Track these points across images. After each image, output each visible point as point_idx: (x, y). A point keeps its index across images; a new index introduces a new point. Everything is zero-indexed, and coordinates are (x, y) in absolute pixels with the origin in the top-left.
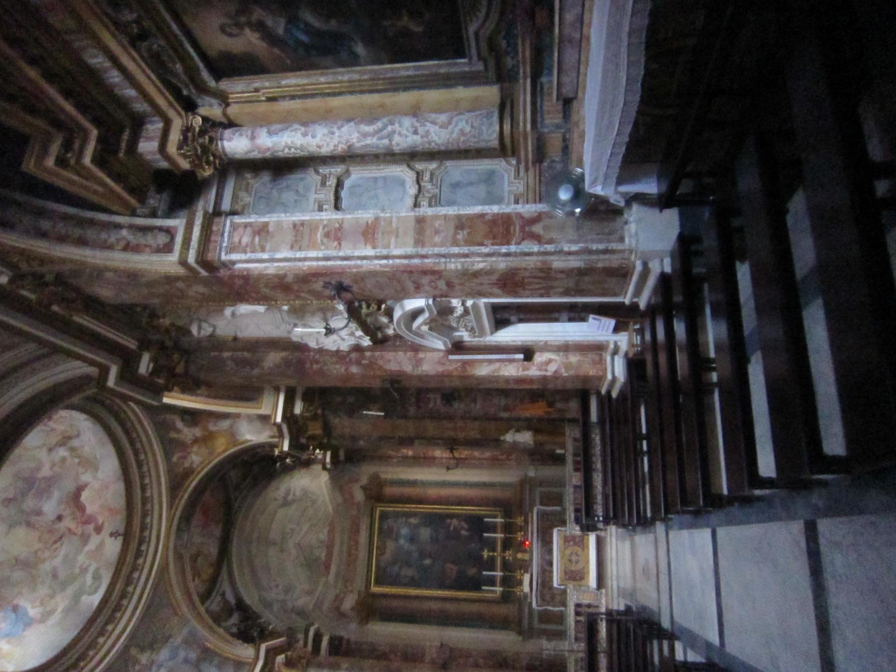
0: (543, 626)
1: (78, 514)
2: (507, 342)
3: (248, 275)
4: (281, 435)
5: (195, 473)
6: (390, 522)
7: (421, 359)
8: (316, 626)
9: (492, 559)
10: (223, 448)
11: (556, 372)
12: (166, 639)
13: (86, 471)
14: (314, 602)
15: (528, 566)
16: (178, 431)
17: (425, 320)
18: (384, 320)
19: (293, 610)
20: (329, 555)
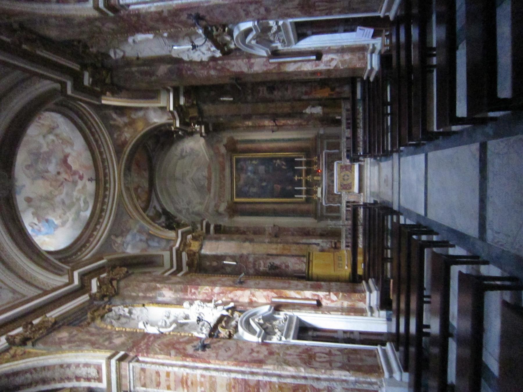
1: (68, 171)
4: (174, 118)
6: (242, 163)
8: (207, 220)
11: (336, 66)
12: (128, 231)
13: (67, 147)
16: (115, 120)
18: (228, 38)
20: (210, 183)
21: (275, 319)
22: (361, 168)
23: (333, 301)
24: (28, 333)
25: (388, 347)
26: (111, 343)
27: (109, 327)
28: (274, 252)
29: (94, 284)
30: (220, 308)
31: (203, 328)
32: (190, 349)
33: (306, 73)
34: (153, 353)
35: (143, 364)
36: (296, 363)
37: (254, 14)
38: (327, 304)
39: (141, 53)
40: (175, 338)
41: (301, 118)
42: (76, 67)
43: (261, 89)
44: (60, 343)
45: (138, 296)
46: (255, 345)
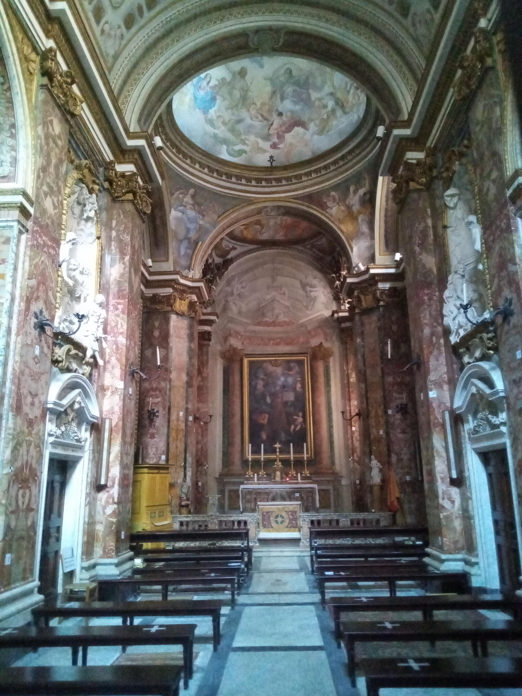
0: (227, 494)
1: (283, 129)
2: (467, 463)
3: (511, 232)
5: (323, 212)
6: (297, 369)
7: (441, 387)
8: (217, 320)
9: (274, 451)
10: (345, 230)
11: (443, 507)
12: (202, 213)
13: (316, 126)
14: (234, 316)
15: (270, 480)
16: (355, 192)
17: (483, 391)
18: (478, 354)
19: (227, 301)
20: (267, 324)
21: (79, 425)
22: (295, 542)
23: (104, 508)
24: (59, 78)
25: (38, 598)
26: (46, 194)
27: (67, 191)
28: (173, 417)
29: (128, 168)
30: (96, 346)
31: (67, 324)
32: (35, 307)
33: (431, 462)
34: (32, 254)
35: (15, 241)
36: (16, 460)
37: (515, 391)
38: (101, 500)
39: (453, 231)
40: (53, 285)
41: (363, 453)
42: (431, 142)
43: (404, 395)
44: (46, 124)
45: (111, 229)
46: (43, 398)
